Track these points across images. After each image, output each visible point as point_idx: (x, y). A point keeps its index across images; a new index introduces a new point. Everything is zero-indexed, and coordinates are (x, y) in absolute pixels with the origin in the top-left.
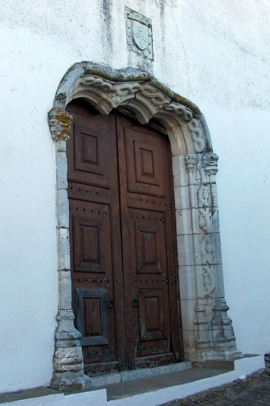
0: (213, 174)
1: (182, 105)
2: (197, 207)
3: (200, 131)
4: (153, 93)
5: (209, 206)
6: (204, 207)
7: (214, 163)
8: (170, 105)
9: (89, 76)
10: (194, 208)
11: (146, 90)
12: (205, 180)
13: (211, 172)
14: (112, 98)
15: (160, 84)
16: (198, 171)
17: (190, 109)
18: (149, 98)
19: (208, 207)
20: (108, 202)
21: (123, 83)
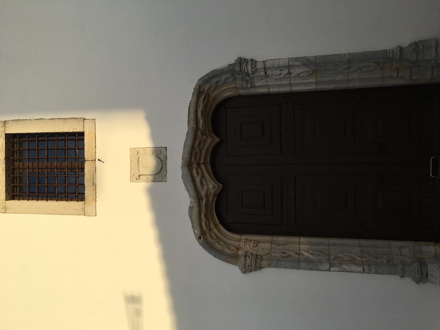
0: (255, 67)
1: (198, 116)
2: (289, 79)
3: (215, 80)
4: (197, 152)
5: (288, 69)
6: (289, 73)
7: (245, 67)
8: (202, 129)
9: (203, 228)
10: (290, 82)
11: (196, 159)
12: (262, 73)
13: (254, 70)
14: (211, 192)
15: (199, 211)
16: (254, 79)
17: (198, 101)
18: (201, 150)
19: (289, 70)
20: (305, 239)
21: (199, 190)
